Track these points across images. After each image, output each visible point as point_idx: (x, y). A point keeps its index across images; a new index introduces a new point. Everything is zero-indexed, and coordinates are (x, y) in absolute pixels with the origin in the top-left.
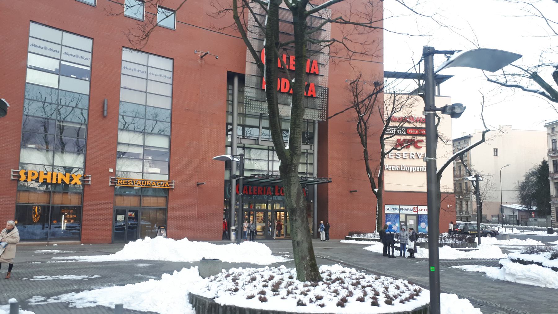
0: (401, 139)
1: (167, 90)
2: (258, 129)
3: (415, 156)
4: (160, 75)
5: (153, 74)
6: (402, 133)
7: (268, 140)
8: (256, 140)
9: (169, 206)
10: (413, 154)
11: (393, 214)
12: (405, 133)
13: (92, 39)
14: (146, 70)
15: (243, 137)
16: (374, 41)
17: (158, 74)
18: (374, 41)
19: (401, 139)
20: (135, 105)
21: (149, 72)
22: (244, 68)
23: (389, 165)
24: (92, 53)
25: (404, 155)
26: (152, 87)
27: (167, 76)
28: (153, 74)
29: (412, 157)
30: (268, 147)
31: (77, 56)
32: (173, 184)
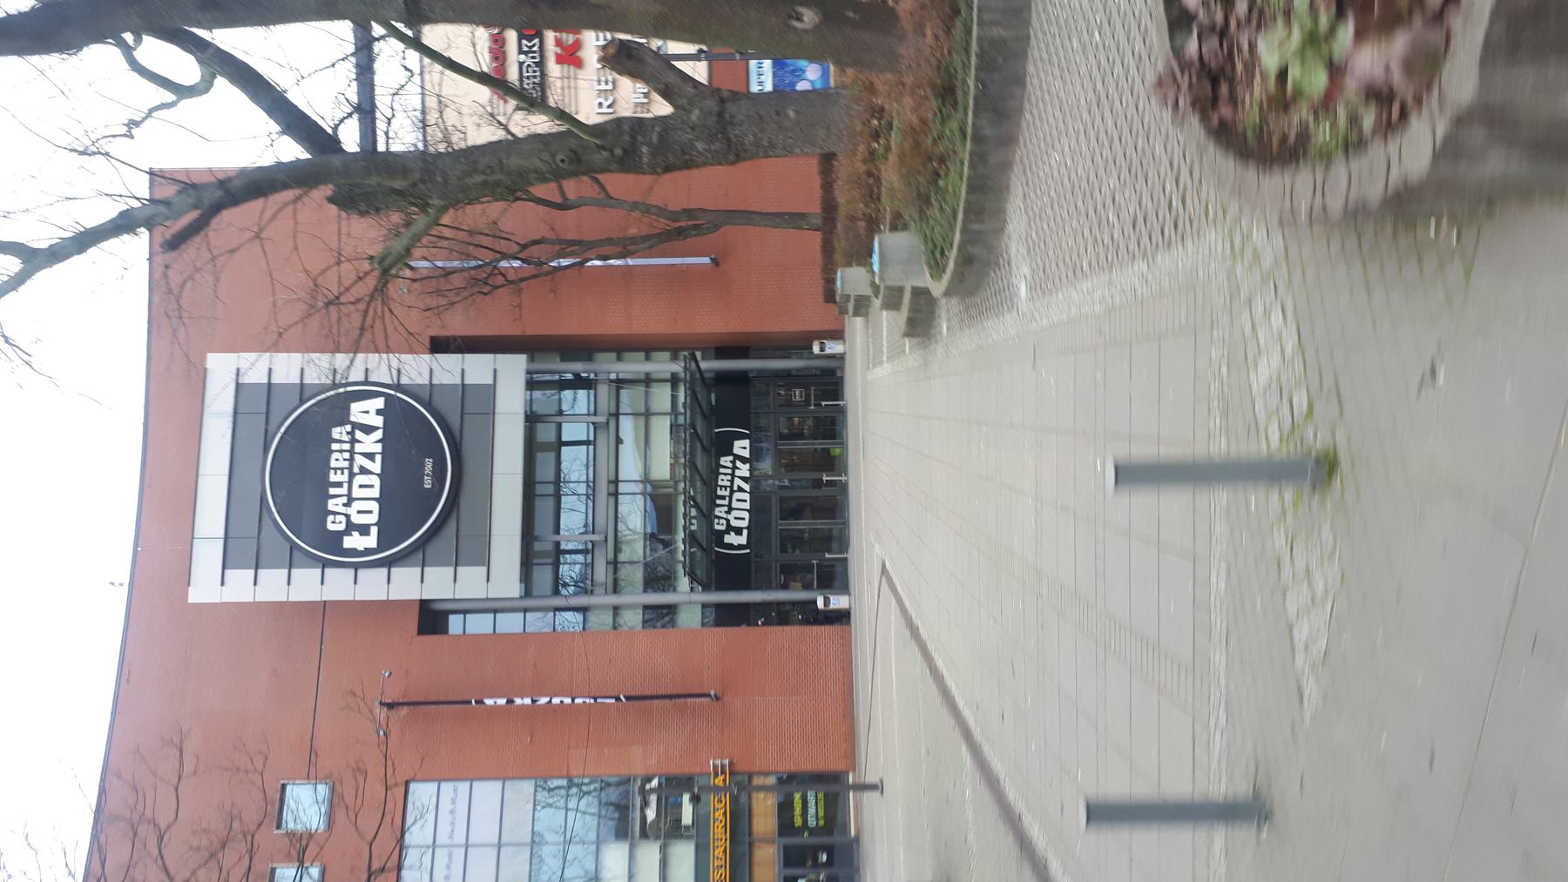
0: (556, 54)
1: (487, 792)
2: (563, 424)
3: (606, 100)
4: (452, 812)
5: (453, 831)
6: (535, 49)
7: (591, 447)
8: (595, 428)
9: (772, 769)
10: (600, 104)
11: (775, 75)
12: (536, 41)
13: (407, 783)
14: (446, 851)
15: (590, 444)
16: (53, 853)
17: (450, 818)
18: (53, 853)
19: (556, 54)
20: (535, 822)
21: (448, 842)
22: (403, 604)
23: (635, 93)
24: (439, 781)
25: (603, 87)
26: (485, 830)
27: (452, 795)
28: (453, 831)
29: (609, 107)
30: (609, 494)
31: (453, 801)
32: (718, 762)
